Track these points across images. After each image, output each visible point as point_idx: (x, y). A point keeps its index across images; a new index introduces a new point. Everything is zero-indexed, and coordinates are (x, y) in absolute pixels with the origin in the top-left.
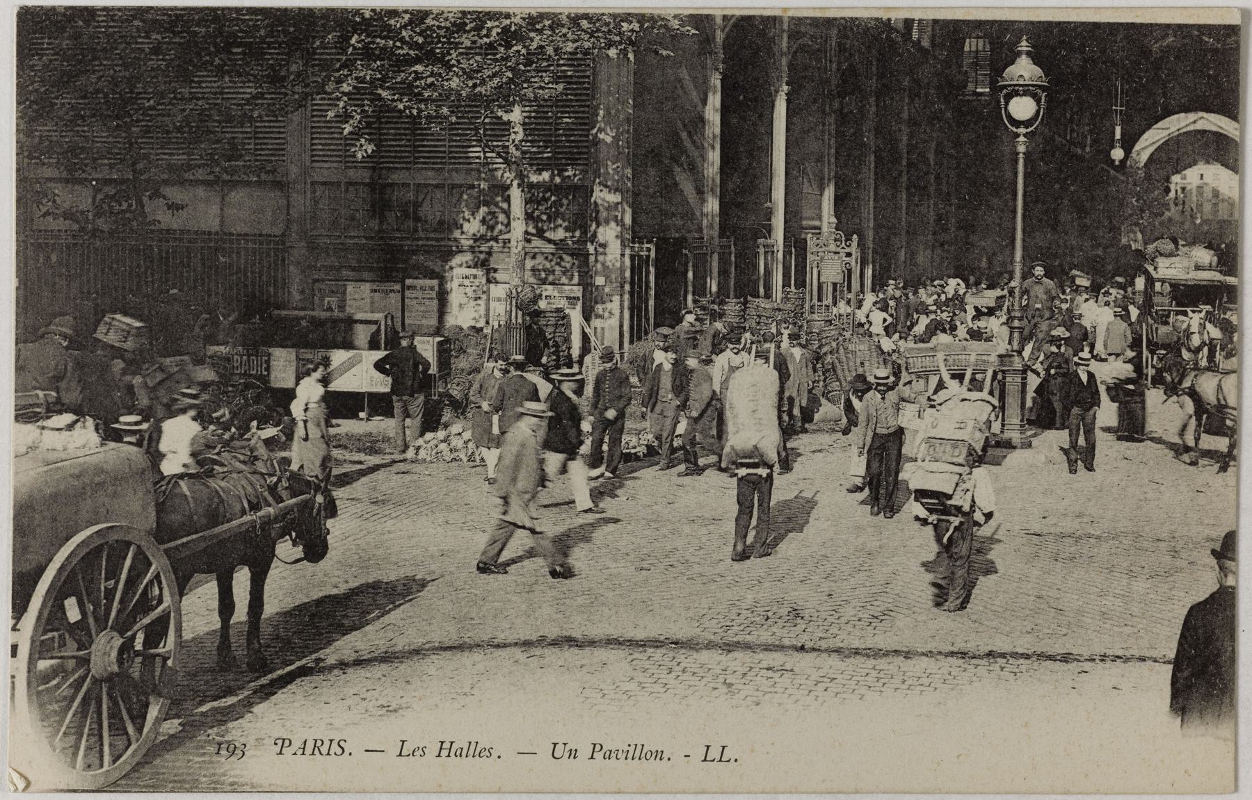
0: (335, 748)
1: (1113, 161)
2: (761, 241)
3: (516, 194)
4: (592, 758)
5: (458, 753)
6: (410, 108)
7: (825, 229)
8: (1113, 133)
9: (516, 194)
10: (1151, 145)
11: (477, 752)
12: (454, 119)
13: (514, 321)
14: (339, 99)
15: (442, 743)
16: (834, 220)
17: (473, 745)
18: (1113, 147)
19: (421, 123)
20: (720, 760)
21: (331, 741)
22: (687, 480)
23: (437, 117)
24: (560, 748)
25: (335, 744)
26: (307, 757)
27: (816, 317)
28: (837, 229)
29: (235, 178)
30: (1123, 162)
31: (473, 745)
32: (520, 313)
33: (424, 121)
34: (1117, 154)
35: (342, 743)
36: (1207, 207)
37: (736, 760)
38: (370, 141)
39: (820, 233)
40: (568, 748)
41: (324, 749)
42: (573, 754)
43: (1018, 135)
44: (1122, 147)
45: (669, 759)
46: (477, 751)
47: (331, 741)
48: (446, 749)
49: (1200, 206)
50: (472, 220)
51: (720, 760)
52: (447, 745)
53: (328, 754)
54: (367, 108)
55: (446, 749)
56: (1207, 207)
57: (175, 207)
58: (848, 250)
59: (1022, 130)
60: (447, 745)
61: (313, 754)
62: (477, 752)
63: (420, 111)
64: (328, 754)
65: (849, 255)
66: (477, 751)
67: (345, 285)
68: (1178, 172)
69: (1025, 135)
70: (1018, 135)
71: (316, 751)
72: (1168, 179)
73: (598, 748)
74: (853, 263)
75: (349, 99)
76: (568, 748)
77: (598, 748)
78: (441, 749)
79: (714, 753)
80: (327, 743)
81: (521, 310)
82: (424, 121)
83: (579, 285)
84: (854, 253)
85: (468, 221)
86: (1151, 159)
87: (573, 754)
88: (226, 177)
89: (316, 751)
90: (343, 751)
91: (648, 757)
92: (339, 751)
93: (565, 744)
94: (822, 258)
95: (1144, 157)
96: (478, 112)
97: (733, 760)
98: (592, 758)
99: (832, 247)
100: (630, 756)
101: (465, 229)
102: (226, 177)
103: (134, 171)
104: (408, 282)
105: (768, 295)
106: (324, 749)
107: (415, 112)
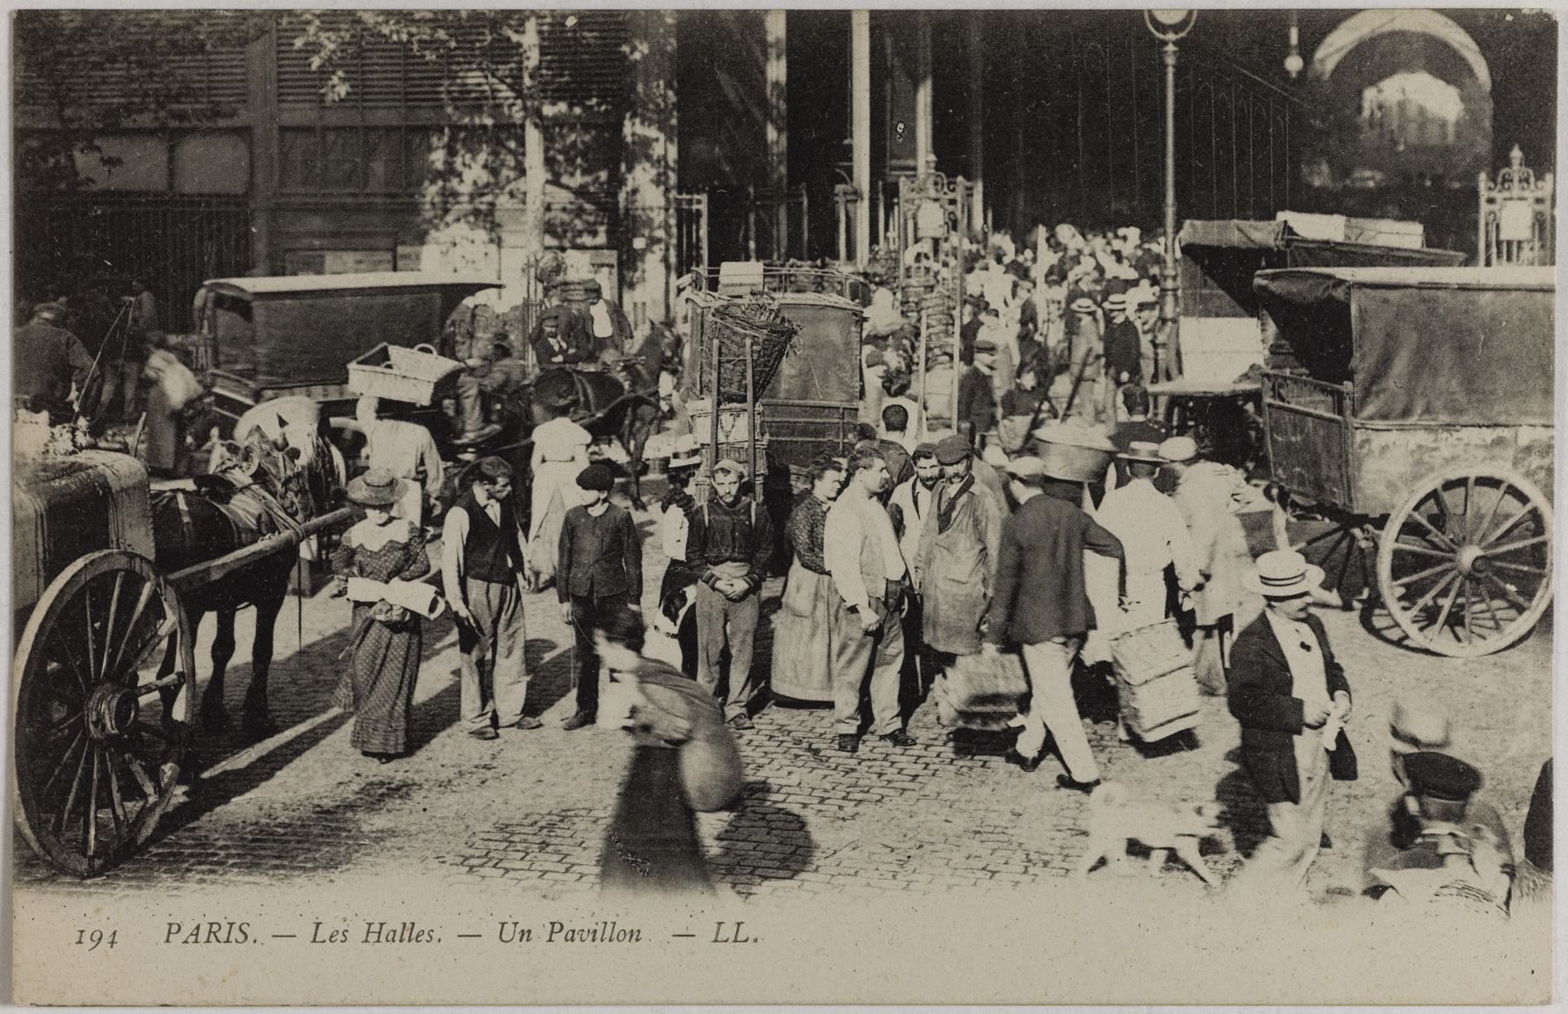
0: (236, 934)
1: (1288, 72)
2: (839, 188)
3: (533, 137)
4: (550, 940)
5: (390, 938)
6: (398, 32)
7: (922, 170)
8: (1287, 37)
9: (533, 137)
10: (1337, 52)
11: (414, 936)
12: (453, 44)
13: (532, 297)
14: (308, 23)
15: (370, 924)
16: (932, 158)
17: (610, 926)
18: (1286, 55)
19: (411, 50)
20: (736, 941)
21: (231, 924)
22: (533, 532)
23: (432, 42)
24: (509, 928)
25: (235, 927)
26: (201, 947)
27: (913, 281)
28: (937, 169)
29: (187, 125)
30: (1302, 74)
31: (610, 926)
32: (540, 286)
33: (415, 47)
34: (1294, 64)
35: (244, 928)
36: (1412, 128)
37: (756, 940)
38: (343, 80)
39: (915, 176)
40: (519, 928)
41: (222, 935)
42: (526, 935)
43: (1165, 43)
44: (1300, 54)
45: (756, 940)
46: (410, 933)
47: (231, 924)
48: (376, 933)
49: (1402, 128)
50: (473, 165)
51: (736, 941)
52: (375, 928)
53: (228, 941)
54: (343, 34)
55: (376, 933)
56: (1412, 128)
57: (110, 162)
58: (951, 196)
59: (1171, 36)
60: (375, 928)
61: (208, 941)
62: (414, 936)
63: (411, 35)
64: (228, 941)
65: (953, 202)
66: (410, 933)
67: (322, 257)
68: (1372, 83)
69: (1175, 43)
70: (1165, 43)
71: (212, 938)
72: (1360, 93)
73: (557, 927)
74: (959, 214)
75: (322, 22)
76: (519, 928)
77: (557, 927)
78: (368, 932)
79: (728, 932)
80: (226, 928)
81: (542, 281)
82: (415, 47)
83: (609, 247)
84: (959, 199)
85: (470, 167)
86: (1337, 69)
87: (526, 935)
88: (175, 124)
89: (212, 938)
90: (246, 938)
91: (621, 937)
92: (241, 937)
93: (516, 924)
94: (919, 207)
95: (1330, 65)
96: (483, 34)
97: (751, 940)
98: (550, 940)
99: (932, 193)
100: (397, 937)
101: (465, 177)
102: (175, 124)
103: (62, 119)
104: (401, 250)
105: (851, 256)
106: (222, 935)
107: (404, 37)
